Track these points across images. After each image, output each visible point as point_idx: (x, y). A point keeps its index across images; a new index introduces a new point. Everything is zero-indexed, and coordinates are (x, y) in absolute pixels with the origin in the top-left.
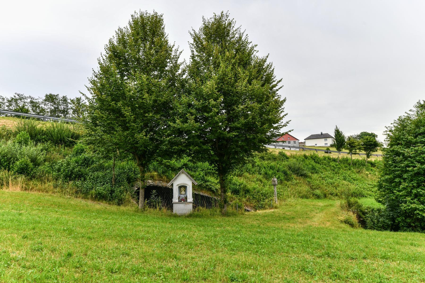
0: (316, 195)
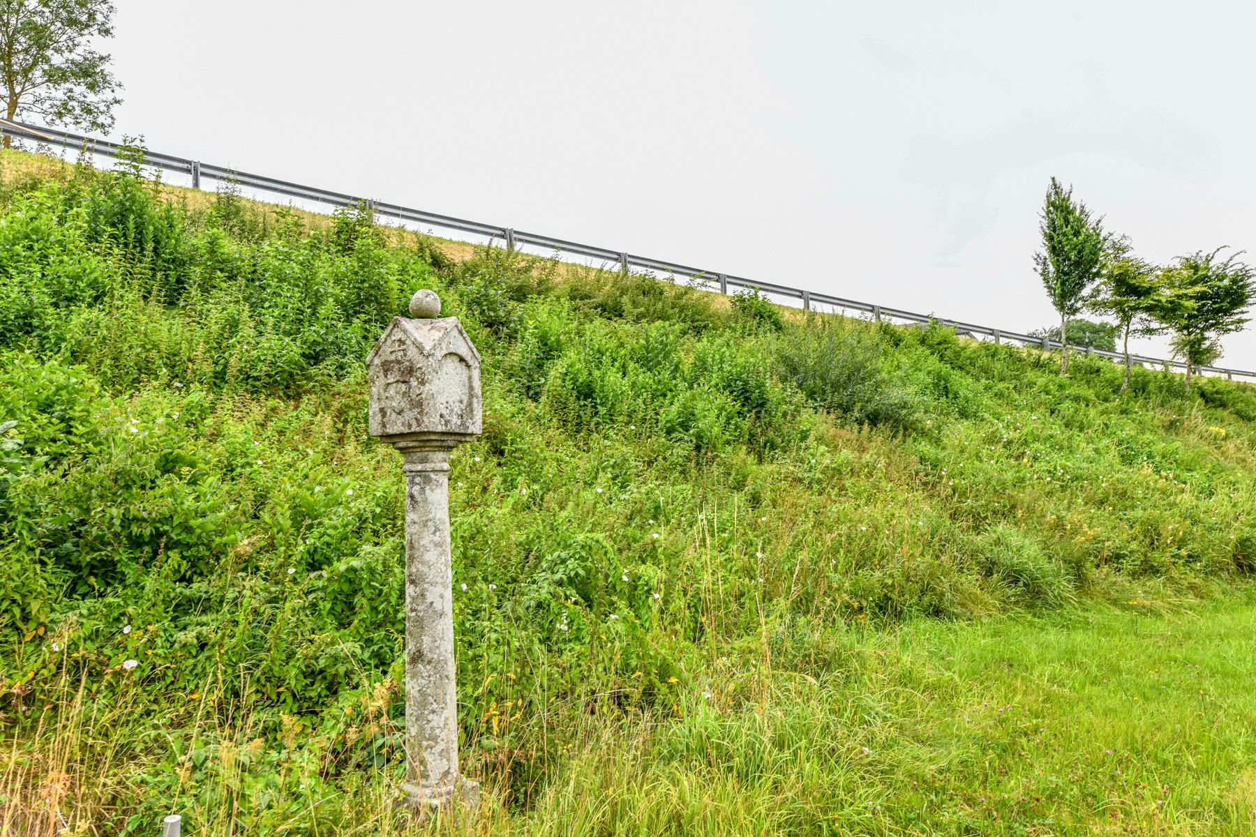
0: (1014, 577)
